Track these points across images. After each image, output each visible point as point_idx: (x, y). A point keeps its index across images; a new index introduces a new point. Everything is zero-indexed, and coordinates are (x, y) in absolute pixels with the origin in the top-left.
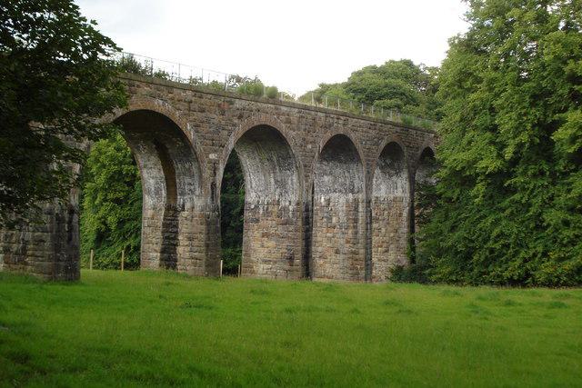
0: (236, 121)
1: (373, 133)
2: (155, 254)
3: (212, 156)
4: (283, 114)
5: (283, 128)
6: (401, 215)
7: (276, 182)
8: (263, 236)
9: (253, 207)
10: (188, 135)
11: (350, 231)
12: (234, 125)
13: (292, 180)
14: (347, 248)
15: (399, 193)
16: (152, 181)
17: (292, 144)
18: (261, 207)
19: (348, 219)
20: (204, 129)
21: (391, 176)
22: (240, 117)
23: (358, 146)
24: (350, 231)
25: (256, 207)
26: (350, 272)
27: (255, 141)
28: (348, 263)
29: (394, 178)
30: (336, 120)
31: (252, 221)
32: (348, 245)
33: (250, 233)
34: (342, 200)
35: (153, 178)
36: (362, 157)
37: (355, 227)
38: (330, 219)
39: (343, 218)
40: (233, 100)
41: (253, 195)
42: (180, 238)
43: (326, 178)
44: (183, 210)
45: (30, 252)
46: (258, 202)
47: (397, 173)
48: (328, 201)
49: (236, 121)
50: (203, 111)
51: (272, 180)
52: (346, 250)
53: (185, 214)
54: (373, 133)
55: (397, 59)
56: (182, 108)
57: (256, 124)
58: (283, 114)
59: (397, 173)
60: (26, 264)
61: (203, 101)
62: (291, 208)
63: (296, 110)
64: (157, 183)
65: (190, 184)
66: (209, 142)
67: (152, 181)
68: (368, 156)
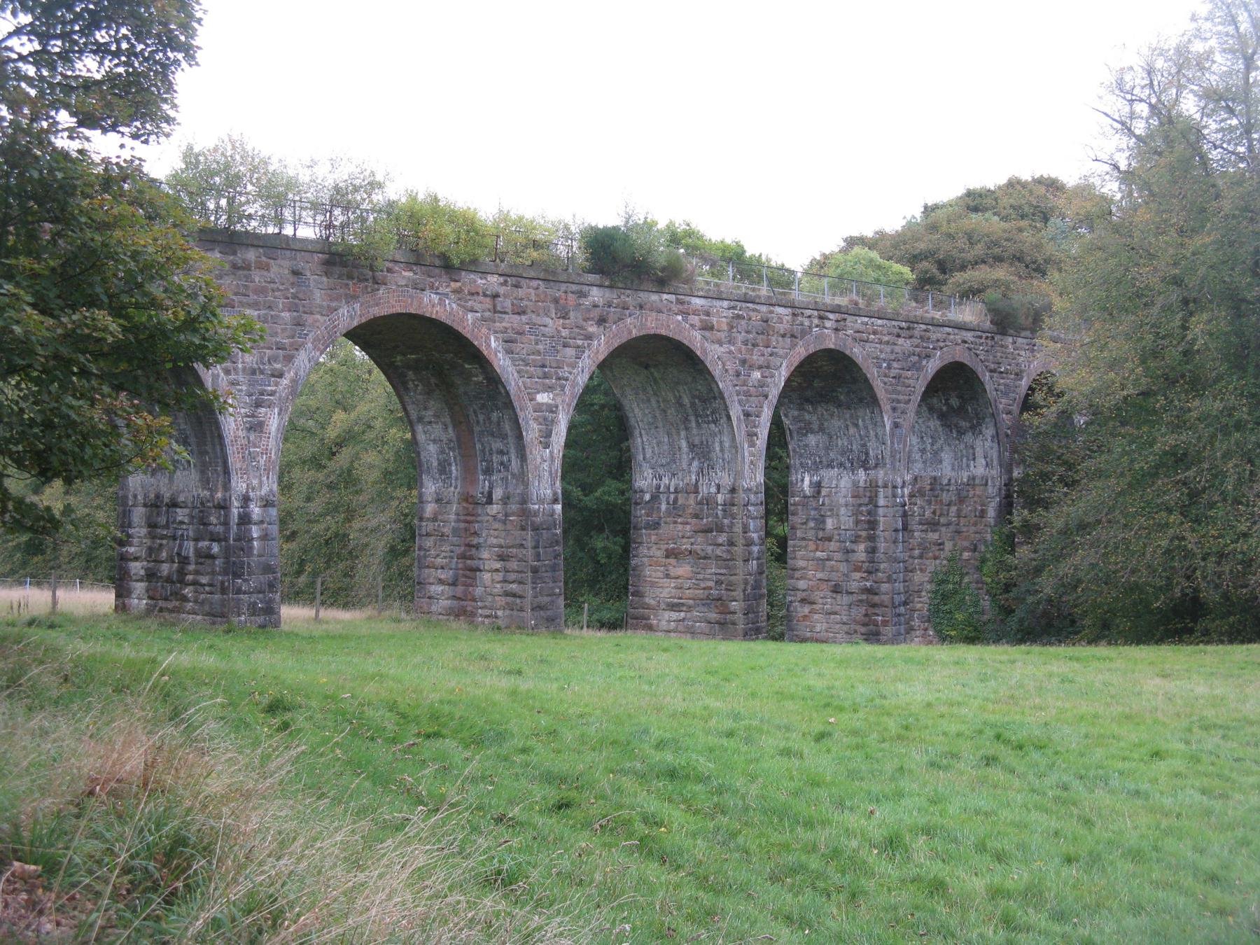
0: (592, 329)
1: (904, 344)
2: (440, 588)
3: (543, 398)
4: (696, 313)
5: (695, 339)
6: (983, 513)
7: (692, 446)
8: (667, 557)
9: (647, 497)
10: (491, 358)
11: (862, 547)
12: (589, 337)
13: (721, 442)
14: (856, 581)
15: (979, 469)
16: (432, 448)
17: (717, 371)
18: (663, 498)
19: (857, 522)
20: (523, 348)
21: (961, 433)
22: (602, 321)
23: (872, 374)
24: (862, 547)
25: (655, 498)
26: (863, 630)
27: (647, 367)
28: (858, 613)
29: (968, 438)
30: (816, 321)
31: (648, 526)
32: (857, 575)
33: (643, 550)
34: (845, 482)
35: (434, 441)
36: (881, 393)
37: (872, 538)
38: (821, 521)
39: (847, 521)
40: (586, 288)
41: (648, 473)
42: (485, 554)
43: (812, 440)
44: (490, 501)
45: (190, 577)
46: (658, 487)
47: (973, 428)
48: (818, 486)
49: (592, 329)
50: (522, 312)
51: (684, 444)
52: (854, 586)
53: (494, 509)
54: (904, 344)
55: (1026, 176)
56: (477, 306)
57: (635, 333)
58: (696, 313)
59: (973, 428)
60: (185, 599)
61: (521, 293)
62: (720, 498)
63: (725, 304)
64: (443, 452)
65: (501, 452)
66: (539, 371)
67: (432, 448)
68: (895, 392)
